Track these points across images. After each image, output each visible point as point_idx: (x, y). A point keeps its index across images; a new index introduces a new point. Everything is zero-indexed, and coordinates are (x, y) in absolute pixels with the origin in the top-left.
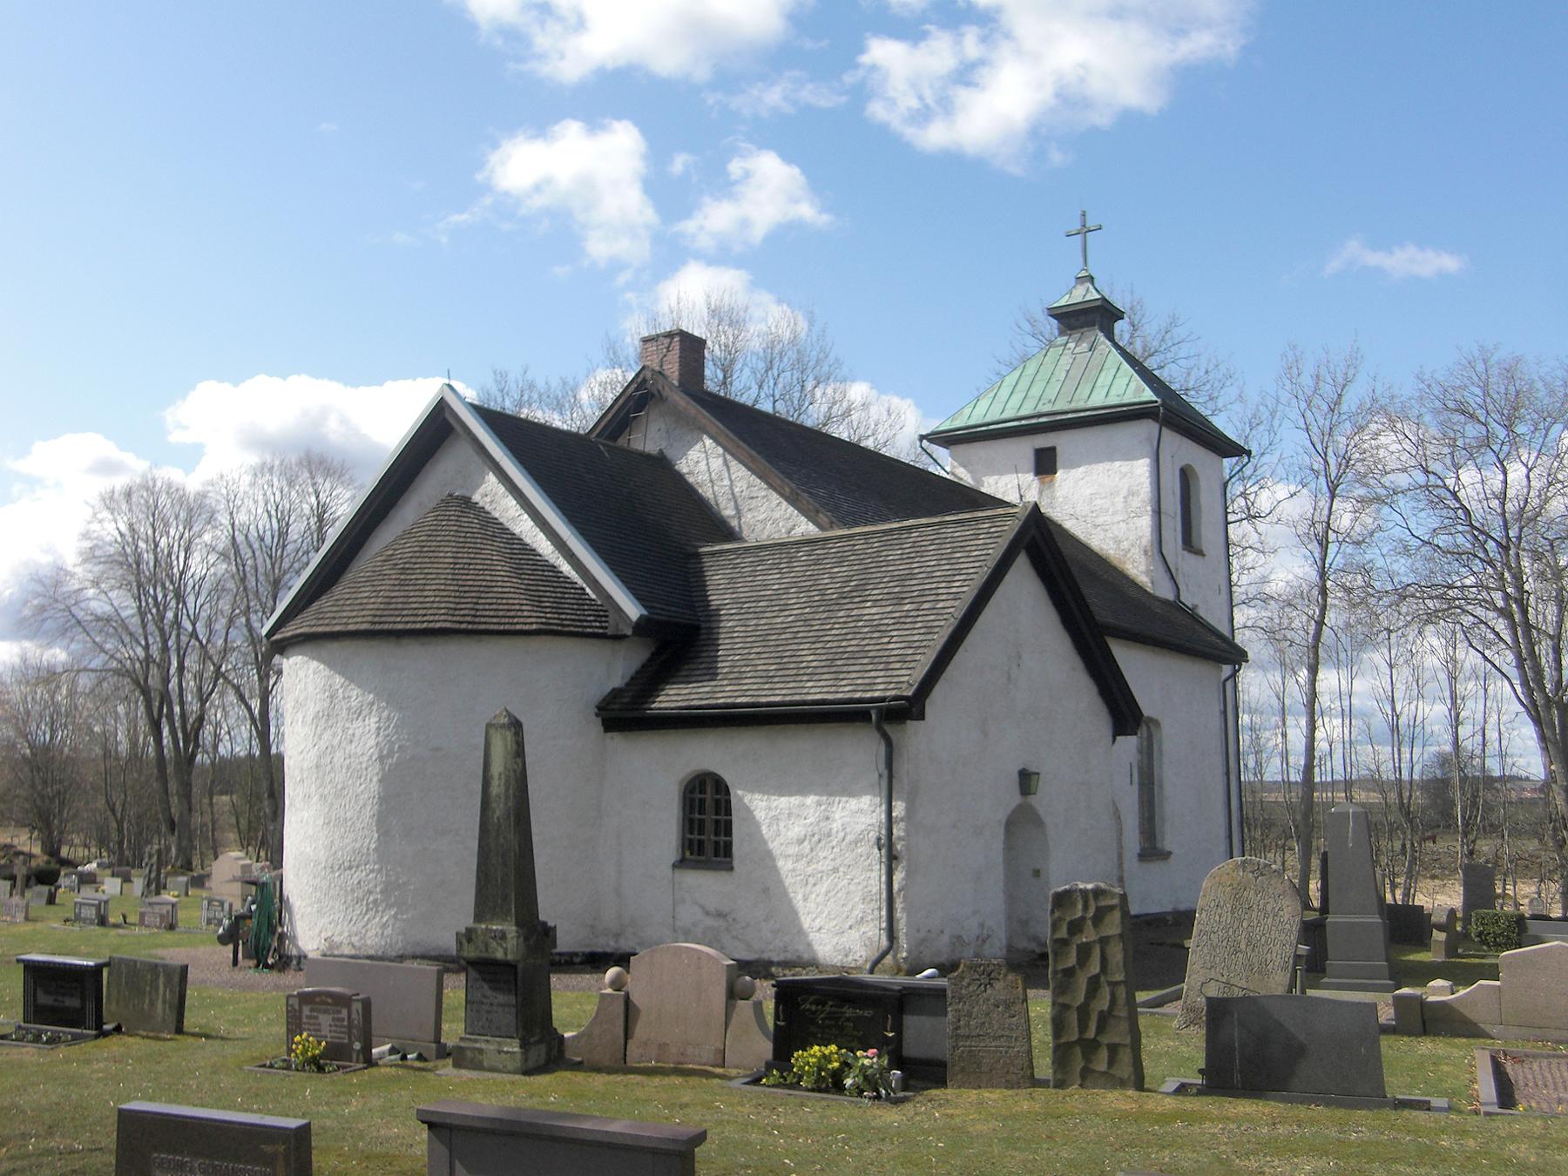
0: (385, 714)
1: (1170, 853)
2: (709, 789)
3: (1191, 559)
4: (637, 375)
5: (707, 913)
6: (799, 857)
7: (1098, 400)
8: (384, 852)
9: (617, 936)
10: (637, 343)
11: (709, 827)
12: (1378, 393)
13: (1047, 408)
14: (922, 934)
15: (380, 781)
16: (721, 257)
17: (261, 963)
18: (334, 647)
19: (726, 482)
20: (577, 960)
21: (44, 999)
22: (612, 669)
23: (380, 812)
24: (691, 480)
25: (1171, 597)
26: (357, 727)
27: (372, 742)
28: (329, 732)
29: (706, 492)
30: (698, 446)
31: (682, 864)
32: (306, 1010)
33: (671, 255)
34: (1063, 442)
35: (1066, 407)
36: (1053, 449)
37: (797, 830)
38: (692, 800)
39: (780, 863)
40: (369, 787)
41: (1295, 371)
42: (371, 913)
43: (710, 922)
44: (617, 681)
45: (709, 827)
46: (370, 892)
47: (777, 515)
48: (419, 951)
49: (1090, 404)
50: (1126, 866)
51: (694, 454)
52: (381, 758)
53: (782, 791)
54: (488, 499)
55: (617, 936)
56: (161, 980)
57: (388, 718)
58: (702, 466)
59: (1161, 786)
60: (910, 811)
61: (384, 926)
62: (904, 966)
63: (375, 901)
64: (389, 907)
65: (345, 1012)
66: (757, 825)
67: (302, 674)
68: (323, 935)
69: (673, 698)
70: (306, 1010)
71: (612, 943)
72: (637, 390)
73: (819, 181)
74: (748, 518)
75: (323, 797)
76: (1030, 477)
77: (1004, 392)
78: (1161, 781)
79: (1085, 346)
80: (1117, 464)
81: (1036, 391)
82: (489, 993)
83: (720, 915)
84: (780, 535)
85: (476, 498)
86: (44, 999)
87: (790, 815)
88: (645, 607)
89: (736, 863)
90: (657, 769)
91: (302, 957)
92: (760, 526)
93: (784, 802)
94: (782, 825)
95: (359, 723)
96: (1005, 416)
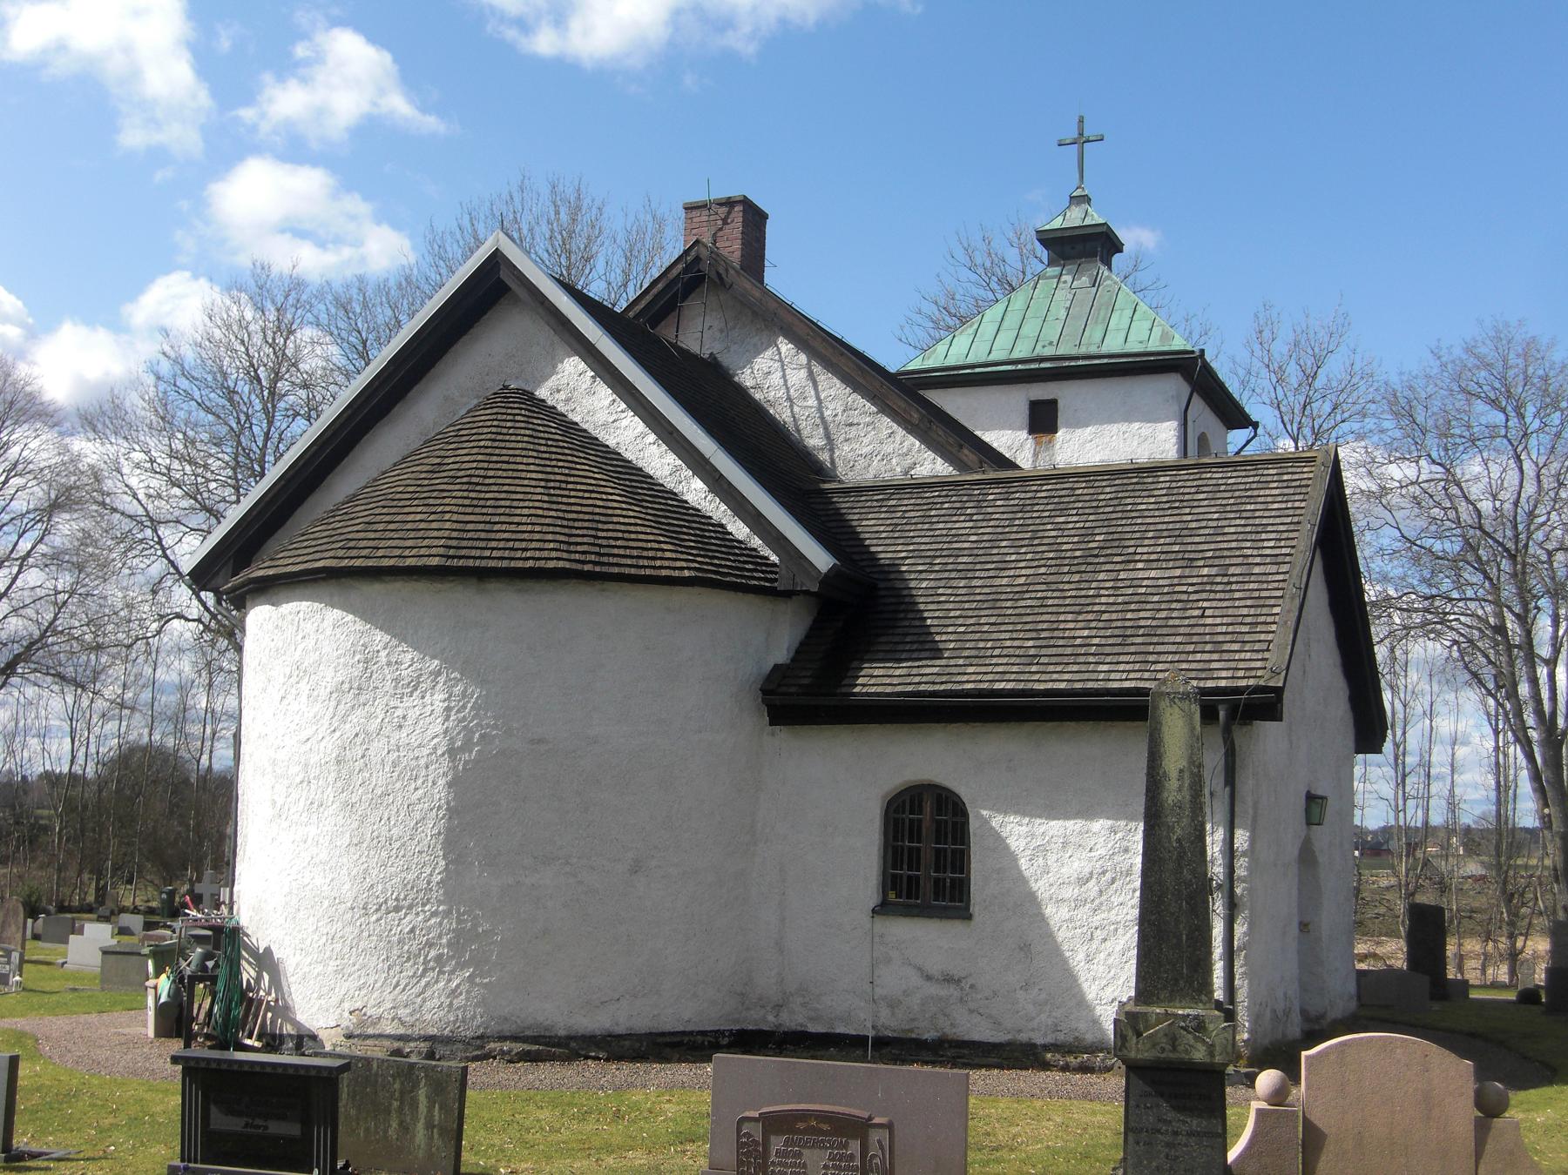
0: (458, 689)
2: (928, 807)
4: (686, 252)
5: (929, 978)
6: (1079, 903)
7: (1114, 344)
8: (454, 888)
11: (927, 857)
12: (1357, 367)
13: (1049, 351)
15: (450, 785)
16: (294, 148)
18: (375, 589)
19: (812, 402)
20: (725, 1041)
21: (221, 1121)
22: (775, 637)
23: (449, 830)
24: (758, 396)
26: (411, 706)
27: (438, 728)
29: (782, 414)
30: (769, 353)
31: (883, 909)
32: (777, 1143)
33: (228, 146)
34: (1067, 394)
35: (1074, 352)
37: (1077, 865)
38: (896, 821)
39: (1049, 910)
41: (1266, 334)
42: (431, 975)
43: (933, 990)
44: (781, 654)
45: (927, 857)
46: (430, 944)
47: (888, 448)
48: (507, 1029)
49: (1104, 350)
51: (763, 362)
52: (452, 752)
53: (1053, 811)
54: (562, 396)
56: (422, 1094)
58: (776, 378)
60: (1253, 840)
61: (454, 993)
62: (1245, 1052)
63: (439, 958)
64: (462, 966)
65: (855, 1147)
66: (1014, 859)
67: (309, 627)
68: (347, 1006)
69: (878, 679)
70: (777, 1143)
71: (771, 1018)
72: (685, 271)
73: (411, 75)
74: (844, 451)
75: (349, 806)
76: (1024, 434)
77: (988, 328)
79: (1085, 280)
80: (1136, 425)
81: (1030, 329)
82: (1171, 1115)
83: (949, 979)
84: (893, 470)
85: (542, 393)
86: (221, 1121)
87: (1065, 845)
89: (975, 909)
90: (843, 786)
92: (862, 462)
93: (1056, 827)
94: (1052, 858)
95: (415, 699)
96: (994, 357)
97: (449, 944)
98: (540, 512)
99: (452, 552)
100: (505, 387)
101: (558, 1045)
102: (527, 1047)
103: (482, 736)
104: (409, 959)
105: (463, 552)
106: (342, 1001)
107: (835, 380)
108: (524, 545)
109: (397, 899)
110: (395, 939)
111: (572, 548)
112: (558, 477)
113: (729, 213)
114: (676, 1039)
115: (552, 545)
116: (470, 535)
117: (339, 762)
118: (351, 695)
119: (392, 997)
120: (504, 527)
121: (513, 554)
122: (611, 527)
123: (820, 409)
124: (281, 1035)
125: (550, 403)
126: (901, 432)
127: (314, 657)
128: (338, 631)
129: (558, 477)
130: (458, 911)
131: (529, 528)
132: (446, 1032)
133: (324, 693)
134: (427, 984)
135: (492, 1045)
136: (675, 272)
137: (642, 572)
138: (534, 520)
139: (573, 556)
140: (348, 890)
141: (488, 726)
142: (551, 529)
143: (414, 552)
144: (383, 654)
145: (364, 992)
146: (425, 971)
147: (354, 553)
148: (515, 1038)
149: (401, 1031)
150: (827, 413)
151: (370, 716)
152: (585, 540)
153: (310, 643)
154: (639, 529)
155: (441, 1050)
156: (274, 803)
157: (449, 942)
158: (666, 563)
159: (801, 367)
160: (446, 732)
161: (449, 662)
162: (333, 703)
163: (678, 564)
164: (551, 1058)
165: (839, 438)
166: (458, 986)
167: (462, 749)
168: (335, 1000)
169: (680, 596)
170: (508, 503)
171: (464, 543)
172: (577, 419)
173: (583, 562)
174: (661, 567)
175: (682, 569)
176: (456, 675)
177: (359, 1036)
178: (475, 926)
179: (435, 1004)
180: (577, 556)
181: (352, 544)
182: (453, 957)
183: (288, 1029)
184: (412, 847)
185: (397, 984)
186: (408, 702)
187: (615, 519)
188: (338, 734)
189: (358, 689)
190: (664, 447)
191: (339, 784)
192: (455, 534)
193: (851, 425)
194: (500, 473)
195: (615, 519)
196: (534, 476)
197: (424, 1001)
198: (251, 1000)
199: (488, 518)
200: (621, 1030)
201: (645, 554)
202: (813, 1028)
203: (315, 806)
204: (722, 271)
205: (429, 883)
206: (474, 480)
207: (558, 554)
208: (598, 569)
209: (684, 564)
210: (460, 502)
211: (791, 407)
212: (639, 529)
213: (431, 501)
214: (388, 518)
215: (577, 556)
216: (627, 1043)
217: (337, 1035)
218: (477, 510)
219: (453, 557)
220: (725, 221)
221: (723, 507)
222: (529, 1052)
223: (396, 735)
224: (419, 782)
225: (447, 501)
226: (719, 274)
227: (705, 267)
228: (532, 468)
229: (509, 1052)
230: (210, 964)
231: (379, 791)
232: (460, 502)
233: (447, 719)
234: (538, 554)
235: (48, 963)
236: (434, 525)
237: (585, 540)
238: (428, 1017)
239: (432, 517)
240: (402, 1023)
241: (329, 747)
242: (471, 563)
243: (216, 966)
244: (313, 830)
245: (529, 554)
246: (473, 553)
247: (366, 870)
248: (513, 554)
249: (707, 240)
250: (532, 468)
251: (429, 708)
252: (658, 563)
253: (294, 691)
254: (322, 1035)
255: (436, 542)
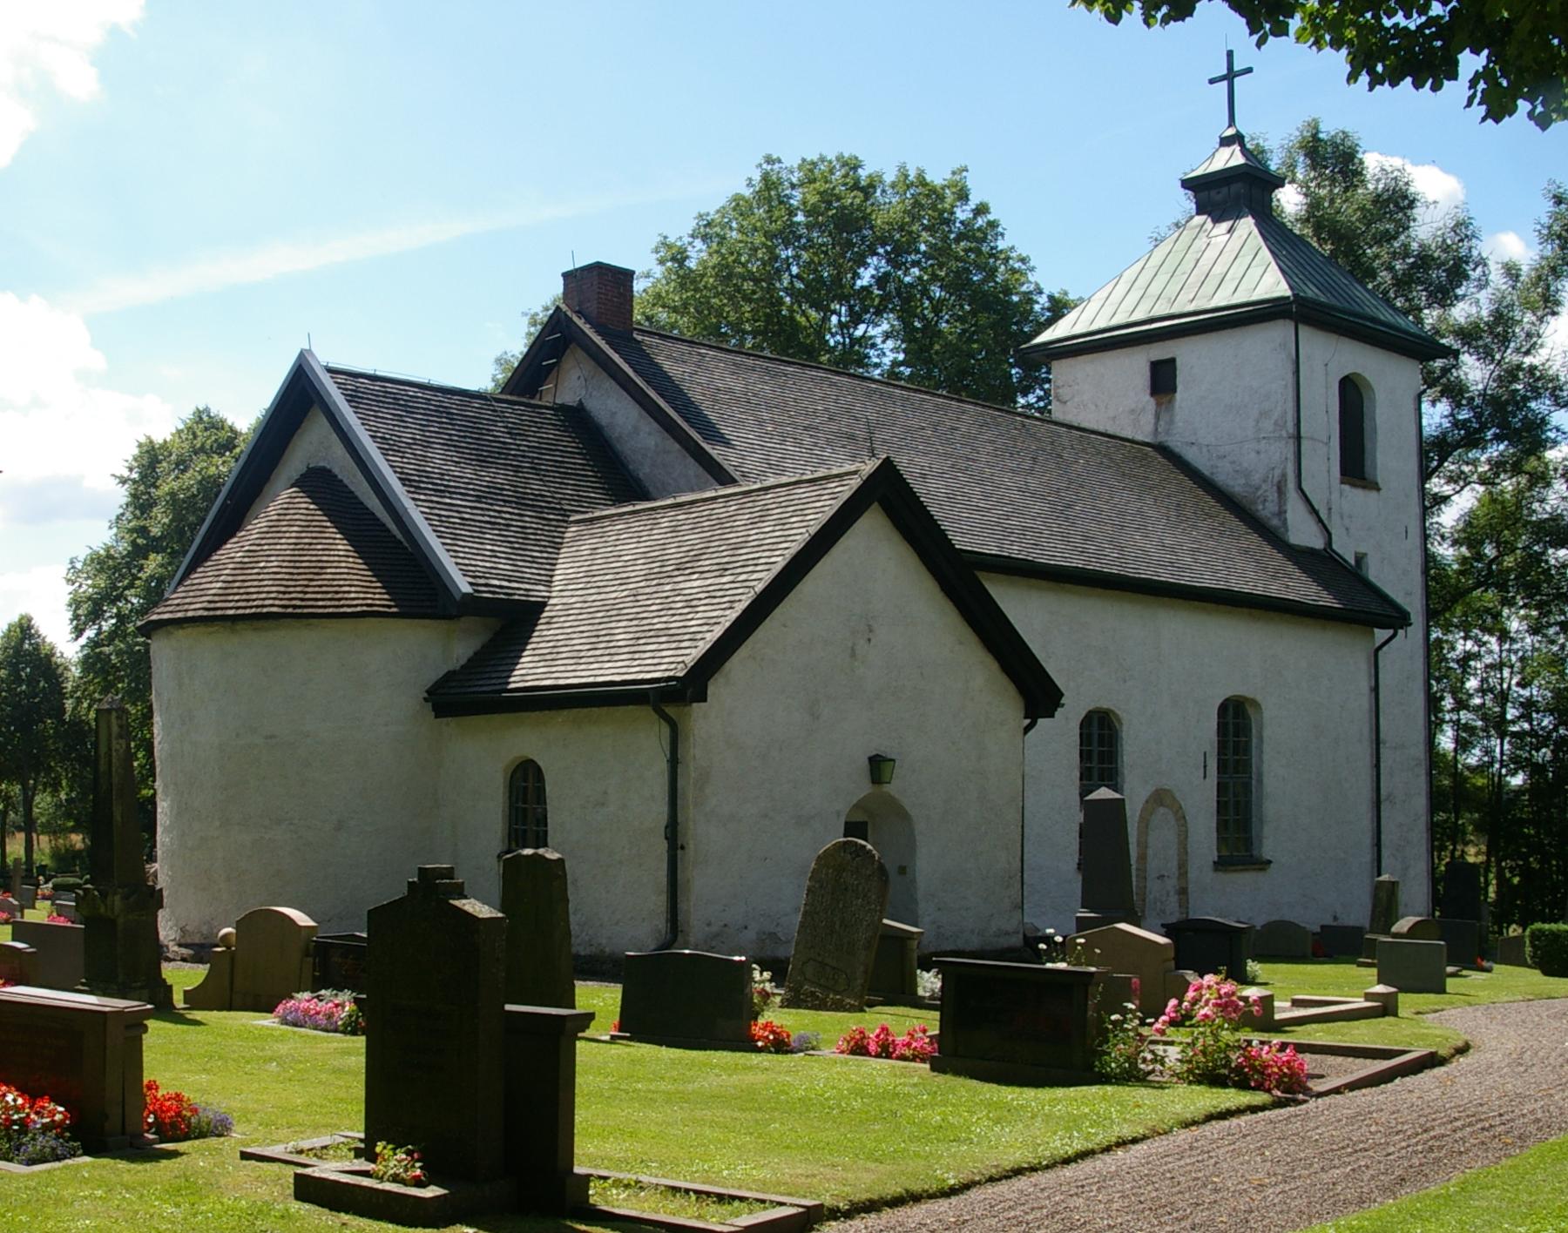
1: (1270, 862)
3: (1356, 496)
14: (714, 929)
25: (1319, 544)
34: (1187, 353)
36: (1172, 361)
50: (1192, 874)
59: (1260, 781)
78: (1260, 775)
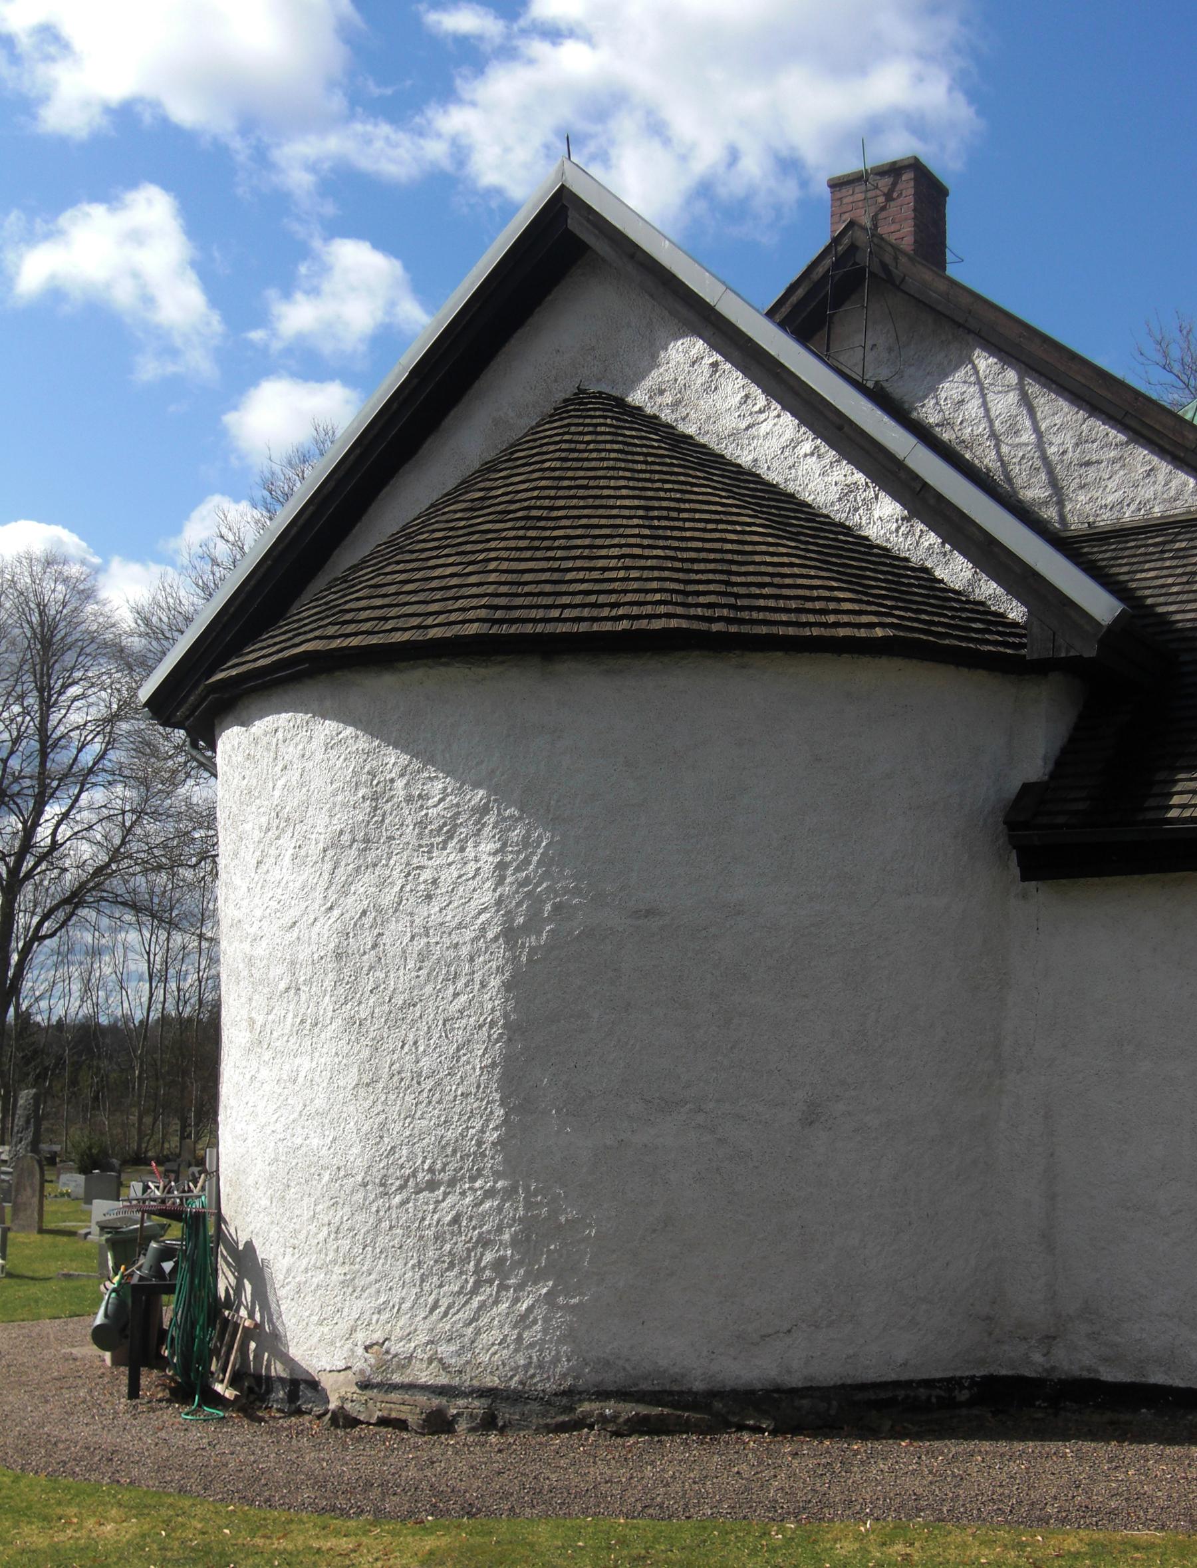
0: (515, 835)
4: (836, 241)
8: (522, 1150)
9: (1049, 1339)
10: (826, 192)
15: (508, 986)
17: (191, 1389)
18: (385, 685)
19: (1028, 436)
20: (964, 1396)
22: (1022, 738)
23: (508, 1059)
26: (444, 864)
27: (486, 897)
28: (368, 877)
30: (960, 374)
40: (484, 997)
42: (487, 1291)
44: (1033, 765)
46: (485, 1242)
48: (611, 1379)
51: (952, 388)
52: (509, 934)
54: (668, 398)
55: (1049, 1339)
57: (525, 842)
58: (973, 408)
61: (523, 1321)
63: (498, 1264)
64: (536, 1277)
67: (291, 752)
68: (361, 1337)
72: (836, 266)
75: (356, 1025)
85: (638, 397)
88: (1121, 599)
91: (302, 1386)
95: (451, 854)
97: (514, 1242)
98: (638, 551)
99: (499, 614)
100: (581, 391)
101: (693, 1406)
102: (643, 1410)
103: (557, 908)
104: (452, 1265)
105: (516, 614)
106: (353, 1330)
107: (1062, 402)
108: (613, 598)
109: (431, 1170)
110: (429, 1233)
111: (690, 600)
112: (665, 504)
113: (894, 184)
114: (883, 1395)
115: (658, 597)
116: (527, 589)
117: (338, 956)
118: (353, 852)
119: (428, 1324)
120: (581, 575)
121: (595, 613)
122: (751, 568)
123: (1040, 444)
124: (269, 1378)
125: (649, 411)
126: (1164, 468)
127: (300, 795)
128: (333, 753)
129: (665, 504)
130: (527, 1189)
131: (622, 574)
132: (513, 1384)
133: (314, 850)
134: (482, 1306)
135: (586, 1407)
136: (821, 270)
137: (807, 632)
138: (629, 562)
139: (692, 611)
140: (357, 1156)
141: (566, 891)
142: (656, 574)
143: (441, 619)
144: (400, 784)
145: (385, 1316)
146: (478, 1285)
147: (351, 628)
148: (623, 1395)
149: (443, 1380)
150: (1051, 450)
151: (383, 884)
152: (712, 587)
153: (294, 775)
154: (796, 570)
155: (505, 1413)
156: (252, 1021)
157: (514, 1239)
158: (846, 619)
159: (1008, 389)
160: (499, 902)
161: (500, 792)
162: (328, 866)
163: (865, 619)
164: (684, 1427)
165: (1070, 484)
166: (530, 1309)
167: (526, 929)
168: (344, 1327)
169: (868, 675)
170: (587, 542)
171: (519, 601)
172: (691, 430)
173: (711, 620)
174: (836, 625)
175: (871, 626)
176: (512, 811)
177: (379, 1386)
178: (554, 1213)
179: (497, 1338)
180: (699, 611)
181: (348, 617)
182: (520, 1263)
183: (278, 1370)
184: (452, 1086)
185: (435, 1306)
186: (440, 857)
187: (757, 558)
188: (336, 912)
189: (363, 842)
190: (832, 454)
191: (340, 990)
192: (504, 589)
193: (1088, 464)
194: (574, 502)
195: (757, 558)
196: (627, 502)
197: (478, 1332)
198: (226, 1321)
199: (556, 564)
200: (795, 1381)
201: (809, 605)
202: (1108, 1374)
203: (309, 1026)
204: (888, 259)
205: (480, 1143)
206: (534, 513)
207: (670, 609)
208: (733, 629)
209: (875, 619)
210: (512, 544)
211: (997, 447)
212: (796, 570)
213: (468, 548)
214: (403, 577)
215: (699, 611)
216: (805, 1402)
217: (347, 1383)
218: (539, 554)
219: (501, 621)
220: (889, 197)
221: (932, 538)
222: (647, 1418)
223: (423, 911)
224: (460, 984)
225: (493, 544)
226: (884, 266)
227: (864, 258)
228: (624, 492)
229: (615, 1417)
230: (168, 1266)
231: (399, 1000)
232: (512, 544)
233: (500, 881)
234: (636, 610)
235: (71, 1233)
236: (473, 579)
237: (712, 587)
238: (485, 1358)
239: (470, 569)
240: (445, 1367)
241: (324, 933)
242: (529, 628)
243: (174, 1270)
244: (305, 1064)
245: (621, 611)
246: (533, 614)
247: (383, 1124)
248: (595, 613)
249: (866, 221)
250: (624, 492)
251: (472, 866)
252: (832, 618)
253: (273, 851)
254: (326, 1382)
255: (474, 602)
